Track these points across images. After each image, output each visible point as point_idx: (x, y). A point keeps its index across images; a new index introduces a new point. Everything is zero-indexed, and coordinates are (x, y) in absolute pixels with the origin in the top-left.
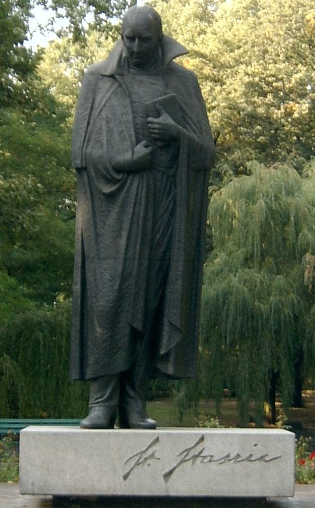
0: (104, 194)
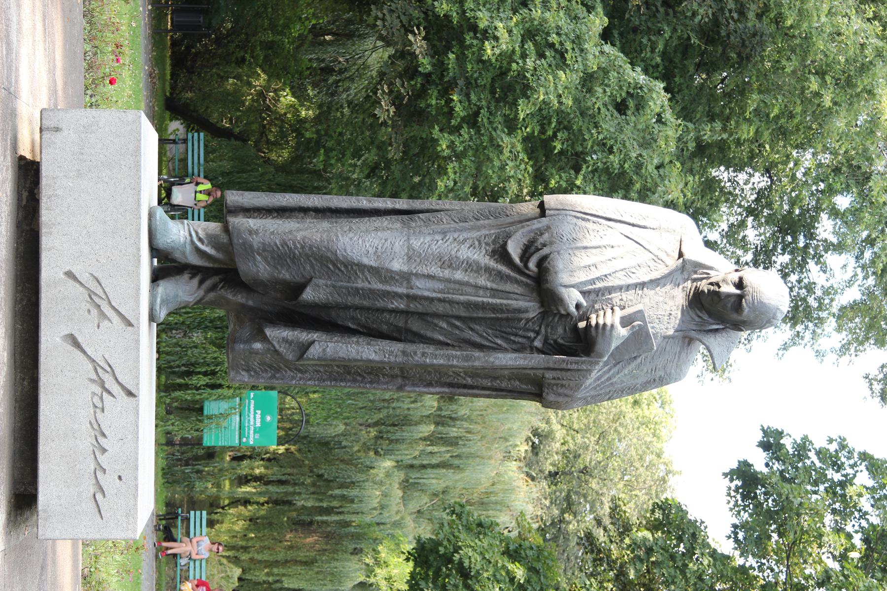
0: (505, 243)
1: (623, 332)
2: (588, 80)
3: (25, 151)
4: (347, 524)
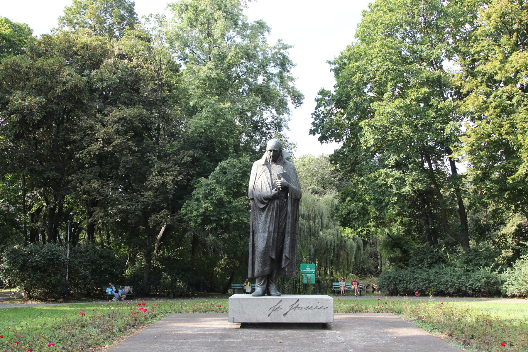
1: (282, 179)
2: (218, 182)
3: (239, 326)
4: (338, 244)
